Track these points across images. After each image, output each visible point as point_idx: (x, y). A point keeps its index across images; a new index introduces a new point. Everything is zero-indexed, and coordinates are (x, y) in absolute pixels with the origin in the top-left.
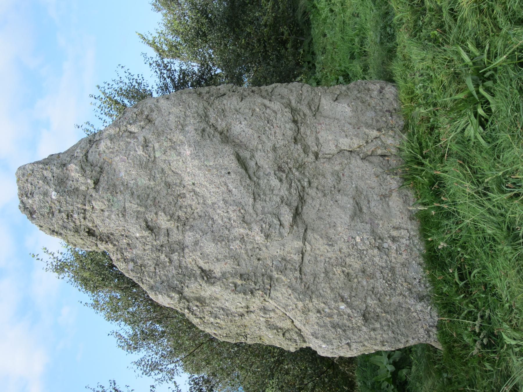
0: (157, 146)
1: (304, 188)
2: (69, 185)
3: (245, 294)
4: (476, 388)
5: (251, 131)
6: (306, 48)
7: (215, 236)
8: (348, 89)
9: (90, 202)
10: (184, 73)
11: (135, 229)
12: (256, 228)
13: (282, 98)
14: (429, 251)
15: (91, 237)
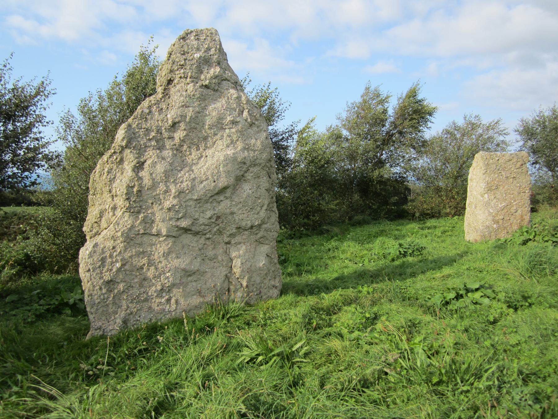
0: (233, 130)
1: (205, 235)
2: (205, 67)
3: (126, 194)
4: (54, 368)
5: (245, 197)
6: (304, 232)
7: (169, 172)
8: (275, 264)
9: (193, 81)
10: (286, 148)
11: (173, 114)
12: (175, 202)
13: (268, 218)
14: (161, 326)
15: (167, 82)
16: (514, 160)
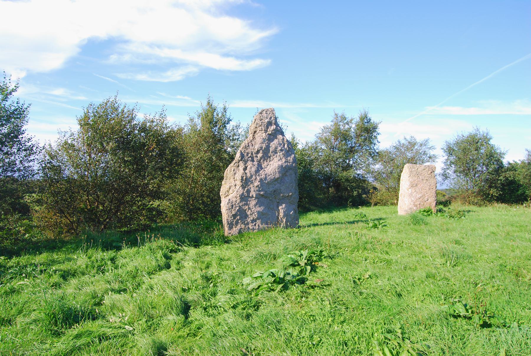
0: (281, 153)
12: (259, 183)
16: (427, 169)
